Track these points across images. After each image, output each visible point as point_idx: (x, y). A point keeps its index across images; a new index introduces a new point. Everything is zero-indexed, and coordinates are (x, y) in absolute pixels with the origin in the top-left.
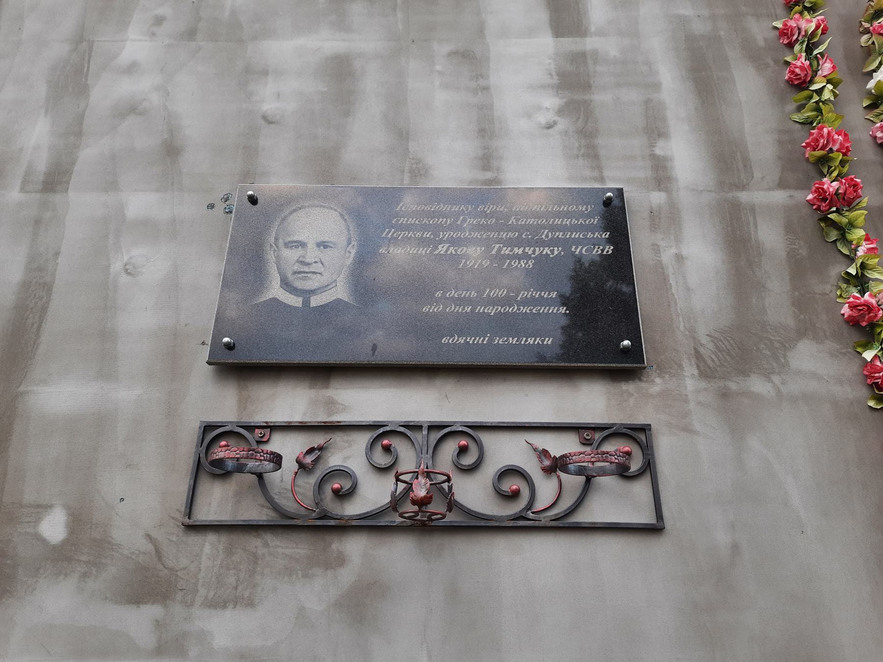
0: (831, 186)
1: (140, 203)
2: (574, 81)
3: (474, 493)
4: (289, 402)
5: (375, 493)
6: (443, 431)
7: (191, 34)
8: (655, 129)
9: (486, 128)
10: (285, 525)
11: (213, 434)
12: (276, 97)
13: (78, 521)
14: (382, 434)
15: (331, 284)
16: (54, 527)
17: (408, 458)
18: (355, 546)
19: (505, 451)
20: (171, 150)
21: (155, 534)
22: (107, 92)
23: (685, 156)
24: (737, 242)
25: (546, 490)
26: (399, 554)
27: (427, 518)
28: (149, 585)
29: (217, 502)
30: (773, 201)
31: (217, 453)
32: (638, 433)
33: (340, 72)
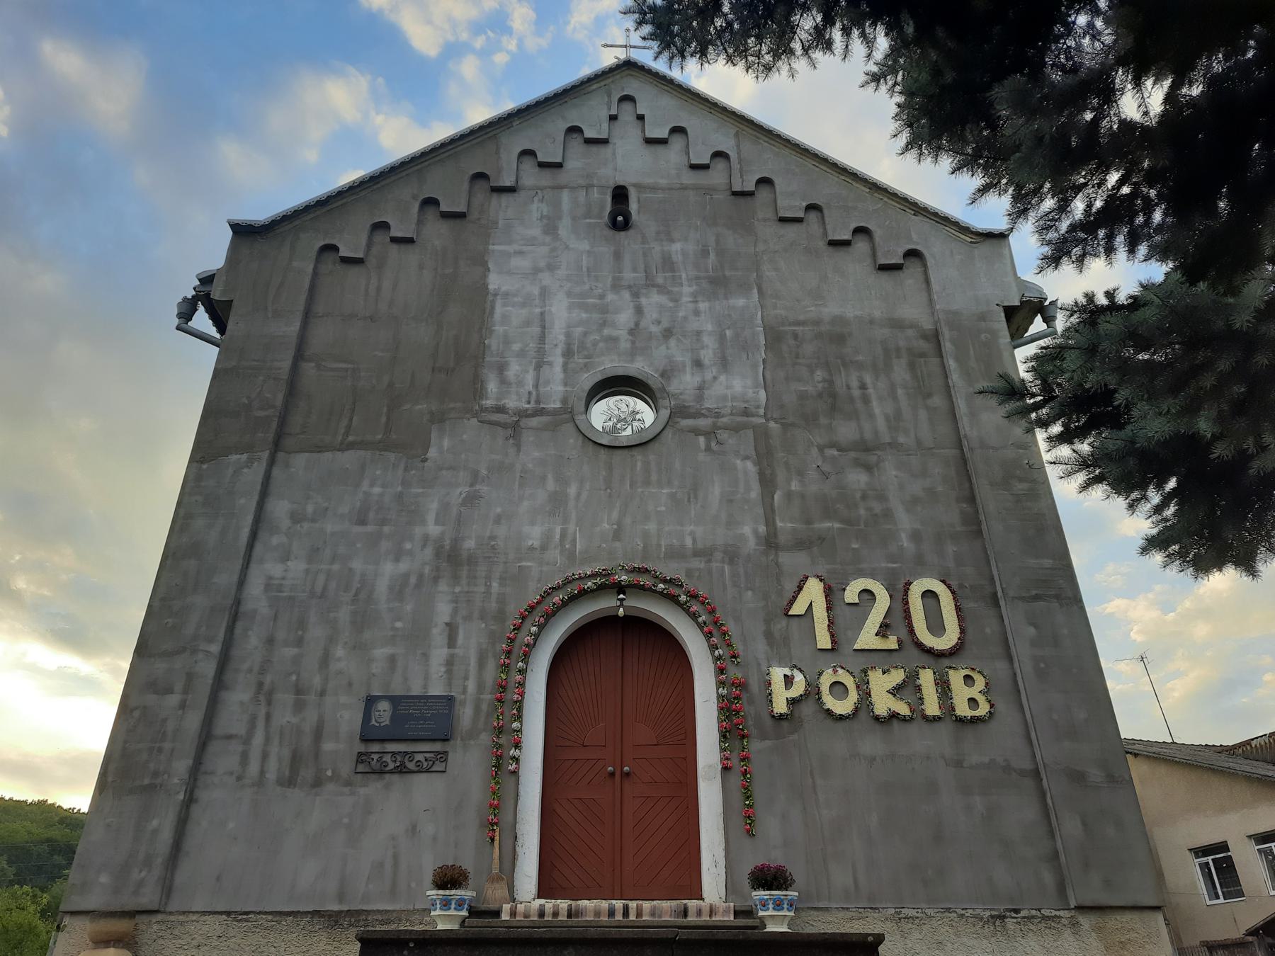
0: (1020, 487)
1: (343, 699)
2: (450, 663)
3: (411, 766)
4: (375, 747)
5: (391, 766)
6: (406, 753)
7: (355, 647)
8: (466, 678)
9: (427, 677)
10: (374, 772)
11: (360, 754)
12: (376, 668)
13: (333, 772)
14: (394, 754)
15: (386, 720)
16: (329, 773)
17: (399, 758)
18: (387, 776)
19: (419, 757)
20: (350, 684)
21: (980, 386)
22: (334, 666)
23: (471, 686)
24: (477, 709)
25: (425, 764)
26: (395, 777)
27: (401, 770)
28: (348, 783)
29: (361, 768)
30: (488, 697)
31: (362, 758)
32: (446, 752)
33: (392, 660)
